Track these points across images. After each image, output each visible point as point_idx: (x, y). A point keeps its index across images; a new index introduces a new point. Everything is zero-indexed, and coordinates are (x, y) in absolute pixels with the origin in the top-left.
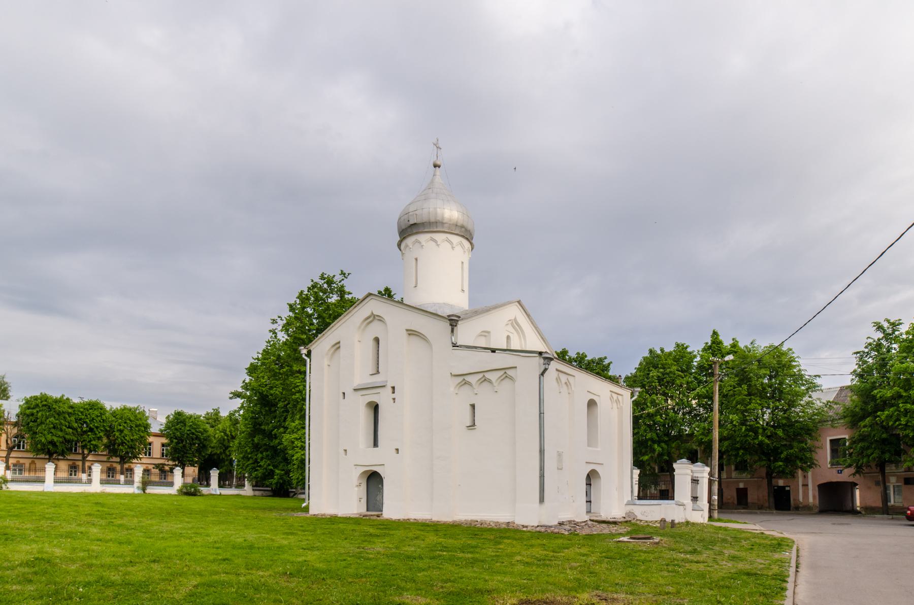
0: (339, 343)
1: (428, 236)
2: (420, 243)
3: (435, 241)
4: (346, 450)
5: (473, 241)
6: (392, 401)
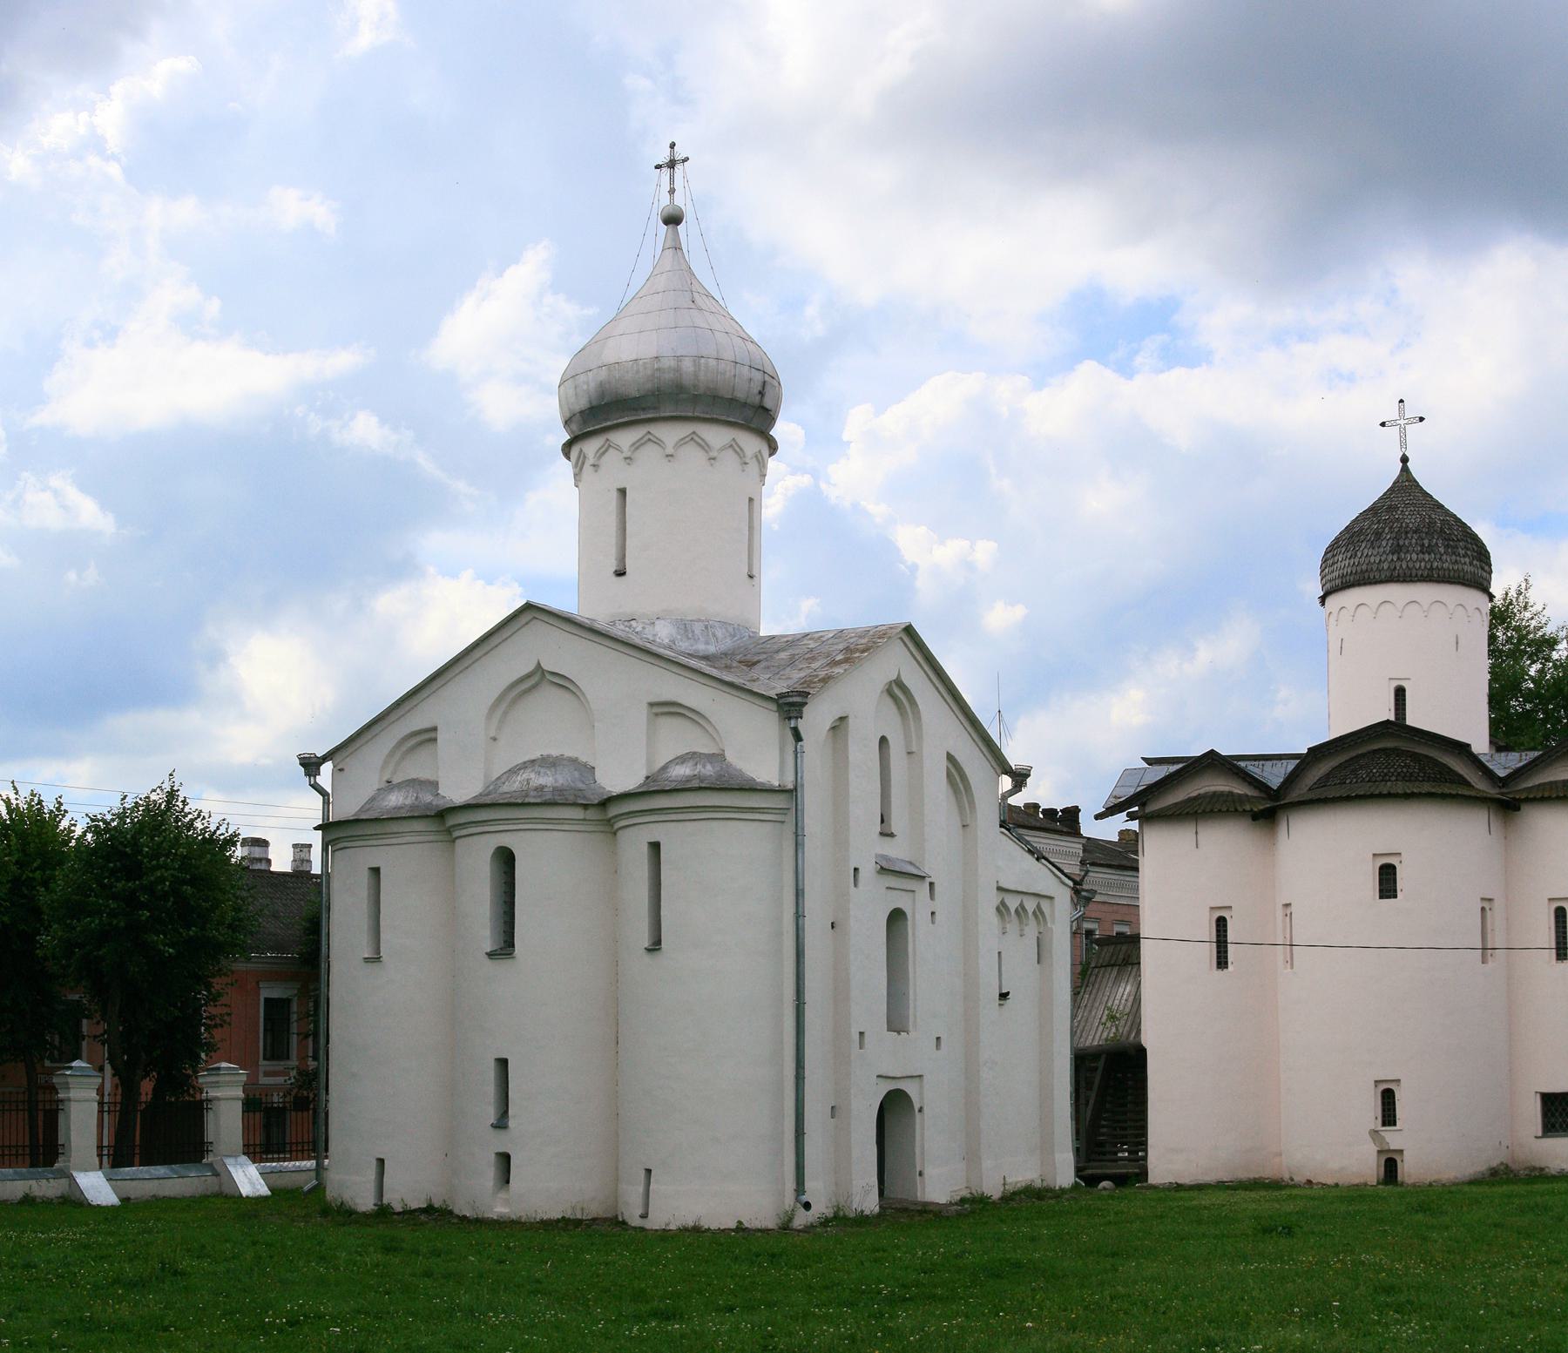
0: (435, 729)
1: (681, 430)
2: (618, 449)
3: (704, 446)
6: (1370, 882)
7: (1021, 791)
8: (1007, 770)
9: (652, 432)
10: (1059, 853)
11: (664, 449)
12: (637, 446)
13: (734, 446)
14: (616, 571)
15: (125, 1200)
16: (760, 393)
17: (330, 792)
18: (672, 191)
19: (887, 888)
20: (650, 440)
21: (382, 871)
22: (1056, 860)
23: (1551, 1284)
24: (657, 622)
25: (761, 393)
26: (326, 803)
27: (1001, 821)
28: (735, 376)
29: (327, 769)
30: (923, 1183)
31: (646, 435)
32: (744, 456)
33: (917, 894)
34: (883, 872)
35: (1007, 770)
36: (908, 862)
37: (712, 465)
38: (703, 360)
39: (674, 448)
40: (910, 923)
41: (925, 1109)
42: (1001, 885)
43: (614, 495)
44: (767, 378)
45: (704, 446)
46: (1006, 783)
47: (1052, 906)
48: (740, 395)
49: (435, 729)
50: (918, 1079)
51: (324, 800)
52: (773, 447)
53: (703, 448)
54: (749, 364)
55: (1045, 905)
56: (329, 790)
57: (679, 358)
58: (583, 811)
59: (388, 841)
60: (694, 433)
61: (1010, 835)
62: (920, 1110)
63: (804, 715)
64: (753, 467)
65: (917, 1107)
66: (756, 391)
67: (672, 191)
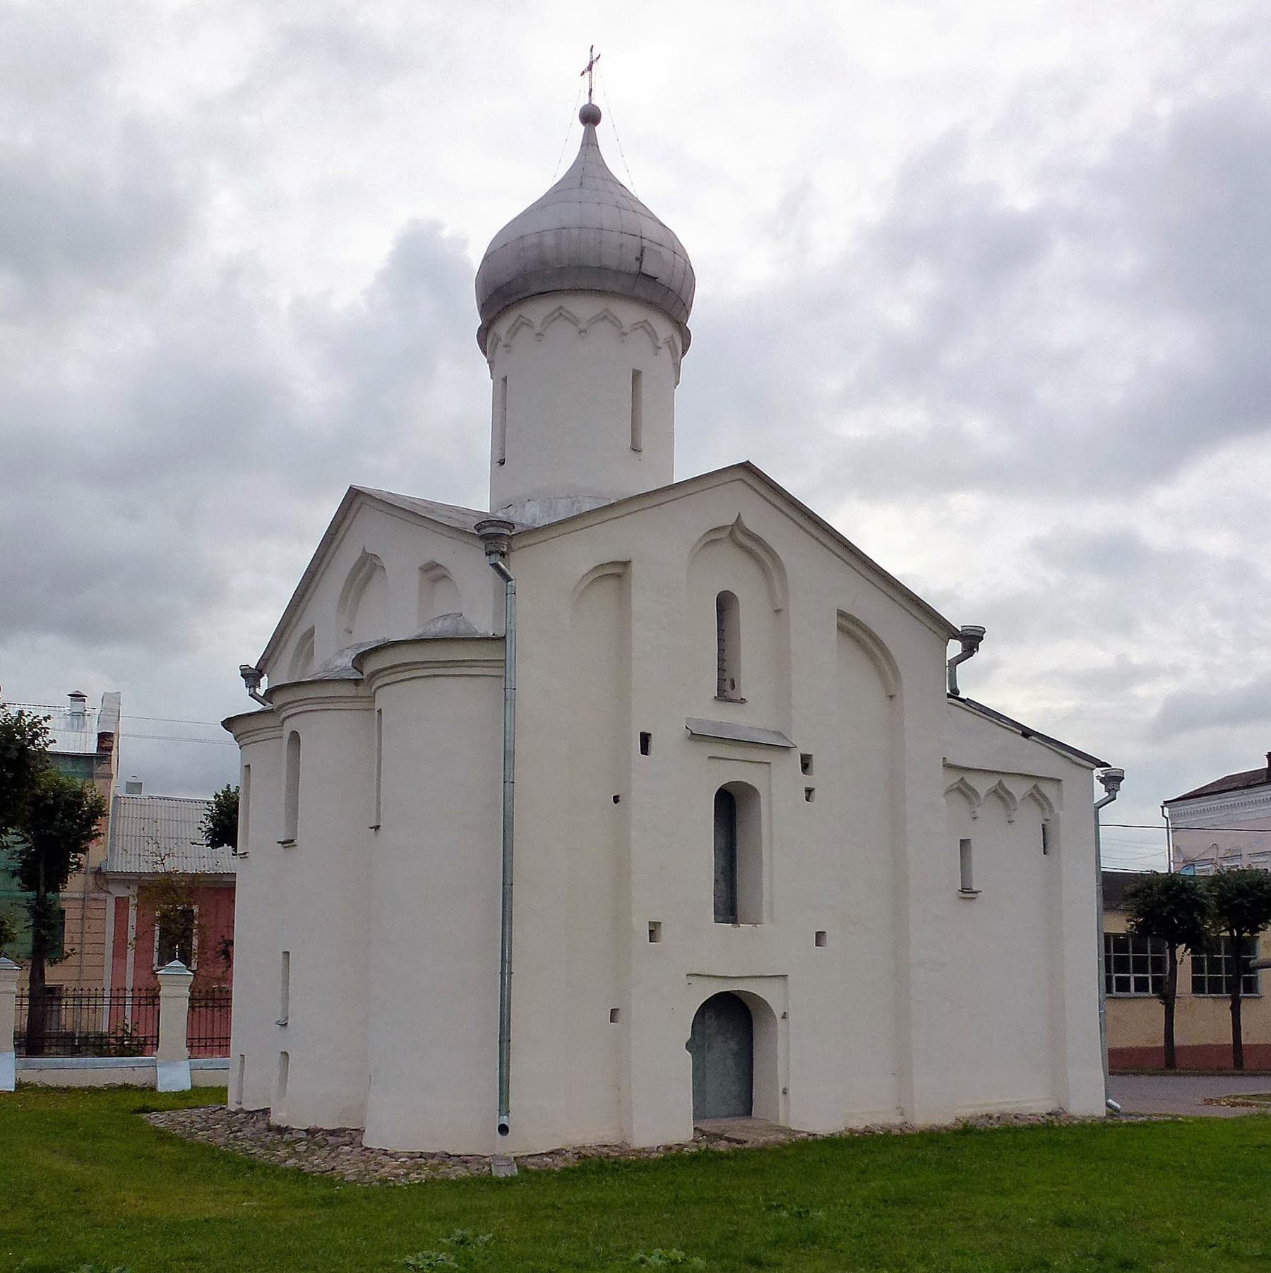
3: (574, 321)
4: (287, 953)
5: (691, 324)
8: (955, 634)
9: (649, 320)
11: (532, 327)
12: (550, 319)
13: (644, 326)
15: (19, 1086)
16: (637, 259)
19: (710, 758)
20: (523, 323)
23: (358, 1228)
24: (528, 505)
25: (640, 260)
28: (600, 243)
30: (787, 1102)
31: (518, 319)
32: (622, 327)
33: (773, 766)
34: (693, 736)
35: (955, 634)
36: (775, 732)
37: (582, 338)
38: (564, 231)
39: (543, 324)
40: (763, 800)
42: (948, 761)
44: (646, 243)
45: (616, 323)
47: (1060, 790)
48: (610, 262)
50: (781, 981)
53: (572, 322)
54: (620, 229)
55: (1048, 789)
57: (540, 233)
58: (355, 687)
59: (254, 739)
60: (561, 307)
61: (968, 708)
64: (665, 352)
65: (778, 1013)
66: (632, 258)
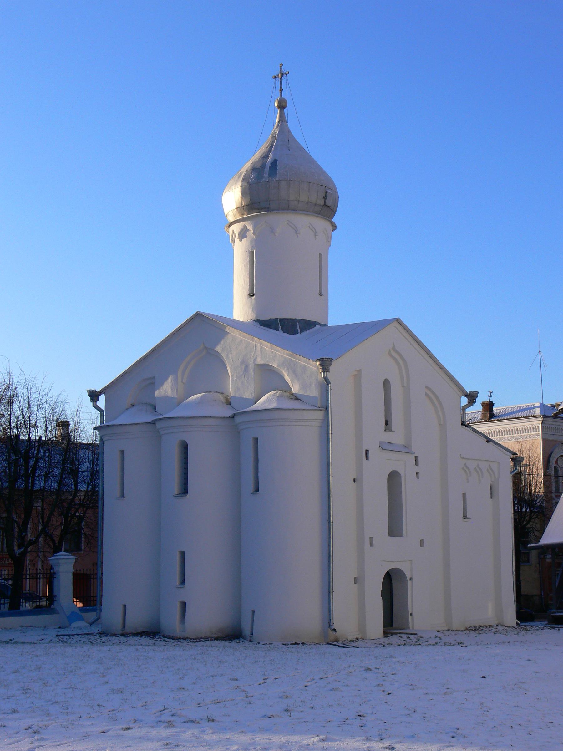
0: (154, 378)
7: (473, 405)
10: (504, 432)
14: (249, 294)
17: (104, 410)
18: (281, 90)
21: (125, 452)
22: (501, 442)
26: (102, 416)
27: (462, 422)
29: (102, 398)
30: (413, 620)
40: (403, 478)
41: (414, 614)
43: (462, 647)
46: (464, 401)
49: (154, 378)
51: (101, 414)
52: (334, 227)
56: (104, 409)
62: (411, 579)
63: (274, 159)
65: (408, 578)
67: (281, 90)
